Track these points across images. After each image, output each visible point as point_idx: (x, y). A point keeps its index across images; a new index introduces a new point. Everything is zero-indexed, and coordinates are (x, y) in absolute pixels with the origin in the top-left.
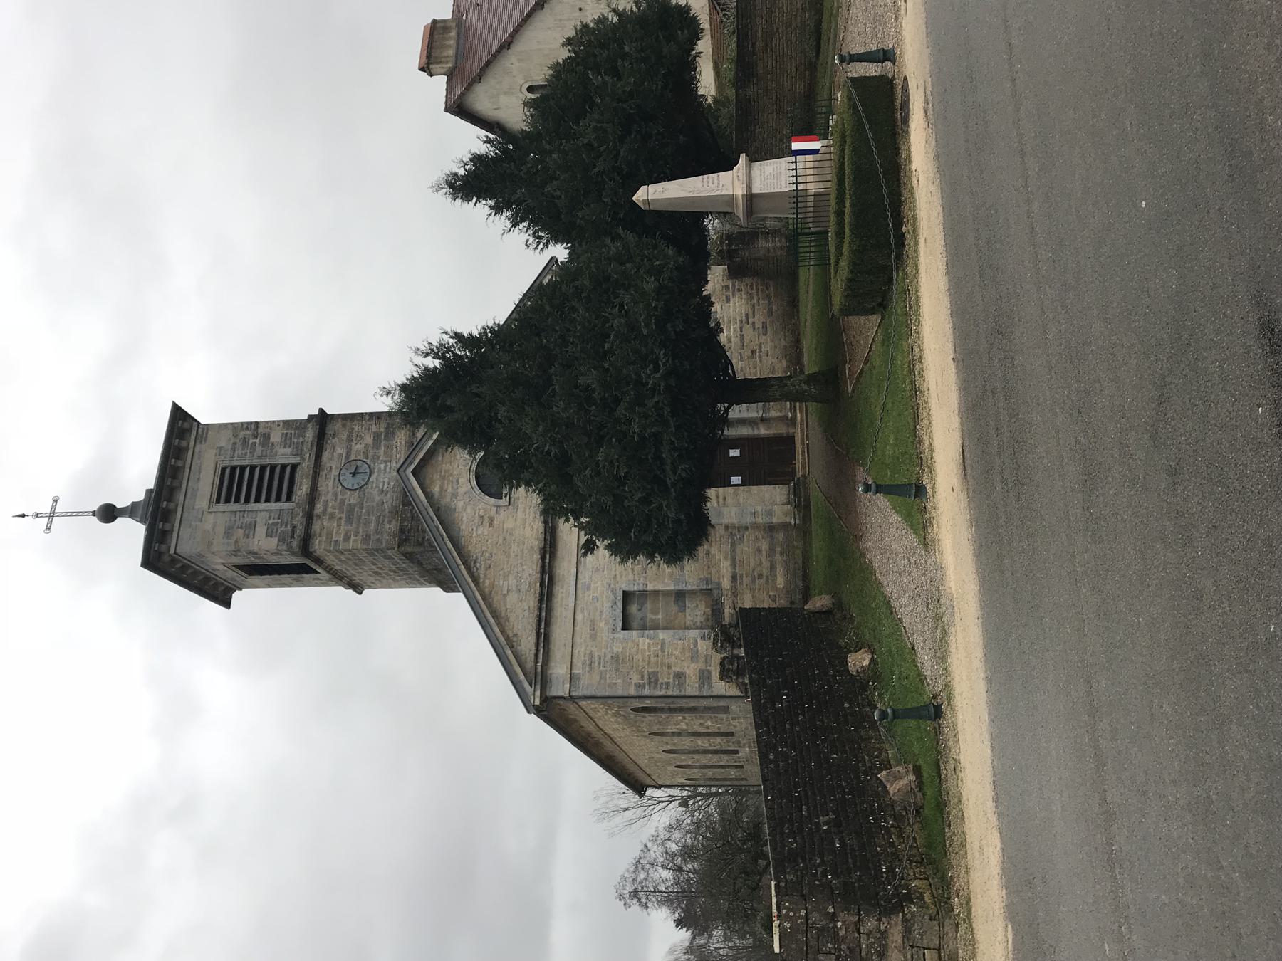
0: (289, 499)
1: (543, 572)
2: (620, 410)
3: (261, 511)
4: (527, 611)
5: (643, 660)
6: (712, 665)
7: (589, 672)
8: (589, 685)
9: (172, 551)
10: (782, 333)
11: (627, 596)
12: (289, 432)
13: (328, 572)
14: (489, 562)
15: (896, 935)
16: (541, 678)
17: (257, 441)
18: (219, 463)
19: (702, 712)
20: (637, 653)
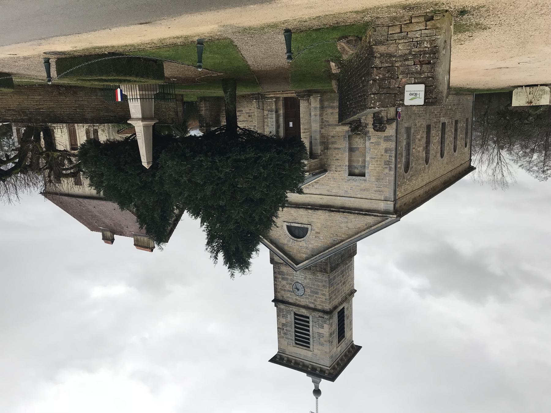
0: (308, 318)
1: (339, 212)
2: (222, 176)
3: (313, 330)
4: (356, 219)
5: (379, 167)
6: (382, 135)
7: (383, 192)
8: (389, 192)
9: (329, 368)
10: (242, 103)
11: (351, 174)
12: (281, 315)
13: (342, 304)
14: (335, 235)
15: (382, 49)
16: (385, 213)
17: (285, 328)
18: (293, 345)
19: (410, 140)
20: (375, 170)
